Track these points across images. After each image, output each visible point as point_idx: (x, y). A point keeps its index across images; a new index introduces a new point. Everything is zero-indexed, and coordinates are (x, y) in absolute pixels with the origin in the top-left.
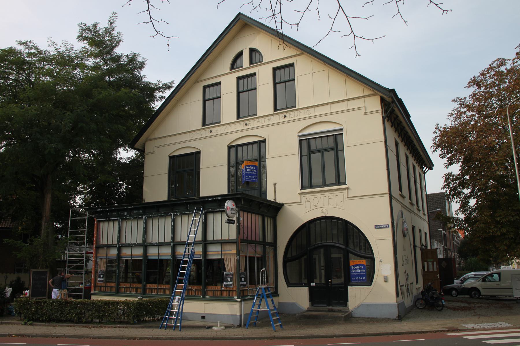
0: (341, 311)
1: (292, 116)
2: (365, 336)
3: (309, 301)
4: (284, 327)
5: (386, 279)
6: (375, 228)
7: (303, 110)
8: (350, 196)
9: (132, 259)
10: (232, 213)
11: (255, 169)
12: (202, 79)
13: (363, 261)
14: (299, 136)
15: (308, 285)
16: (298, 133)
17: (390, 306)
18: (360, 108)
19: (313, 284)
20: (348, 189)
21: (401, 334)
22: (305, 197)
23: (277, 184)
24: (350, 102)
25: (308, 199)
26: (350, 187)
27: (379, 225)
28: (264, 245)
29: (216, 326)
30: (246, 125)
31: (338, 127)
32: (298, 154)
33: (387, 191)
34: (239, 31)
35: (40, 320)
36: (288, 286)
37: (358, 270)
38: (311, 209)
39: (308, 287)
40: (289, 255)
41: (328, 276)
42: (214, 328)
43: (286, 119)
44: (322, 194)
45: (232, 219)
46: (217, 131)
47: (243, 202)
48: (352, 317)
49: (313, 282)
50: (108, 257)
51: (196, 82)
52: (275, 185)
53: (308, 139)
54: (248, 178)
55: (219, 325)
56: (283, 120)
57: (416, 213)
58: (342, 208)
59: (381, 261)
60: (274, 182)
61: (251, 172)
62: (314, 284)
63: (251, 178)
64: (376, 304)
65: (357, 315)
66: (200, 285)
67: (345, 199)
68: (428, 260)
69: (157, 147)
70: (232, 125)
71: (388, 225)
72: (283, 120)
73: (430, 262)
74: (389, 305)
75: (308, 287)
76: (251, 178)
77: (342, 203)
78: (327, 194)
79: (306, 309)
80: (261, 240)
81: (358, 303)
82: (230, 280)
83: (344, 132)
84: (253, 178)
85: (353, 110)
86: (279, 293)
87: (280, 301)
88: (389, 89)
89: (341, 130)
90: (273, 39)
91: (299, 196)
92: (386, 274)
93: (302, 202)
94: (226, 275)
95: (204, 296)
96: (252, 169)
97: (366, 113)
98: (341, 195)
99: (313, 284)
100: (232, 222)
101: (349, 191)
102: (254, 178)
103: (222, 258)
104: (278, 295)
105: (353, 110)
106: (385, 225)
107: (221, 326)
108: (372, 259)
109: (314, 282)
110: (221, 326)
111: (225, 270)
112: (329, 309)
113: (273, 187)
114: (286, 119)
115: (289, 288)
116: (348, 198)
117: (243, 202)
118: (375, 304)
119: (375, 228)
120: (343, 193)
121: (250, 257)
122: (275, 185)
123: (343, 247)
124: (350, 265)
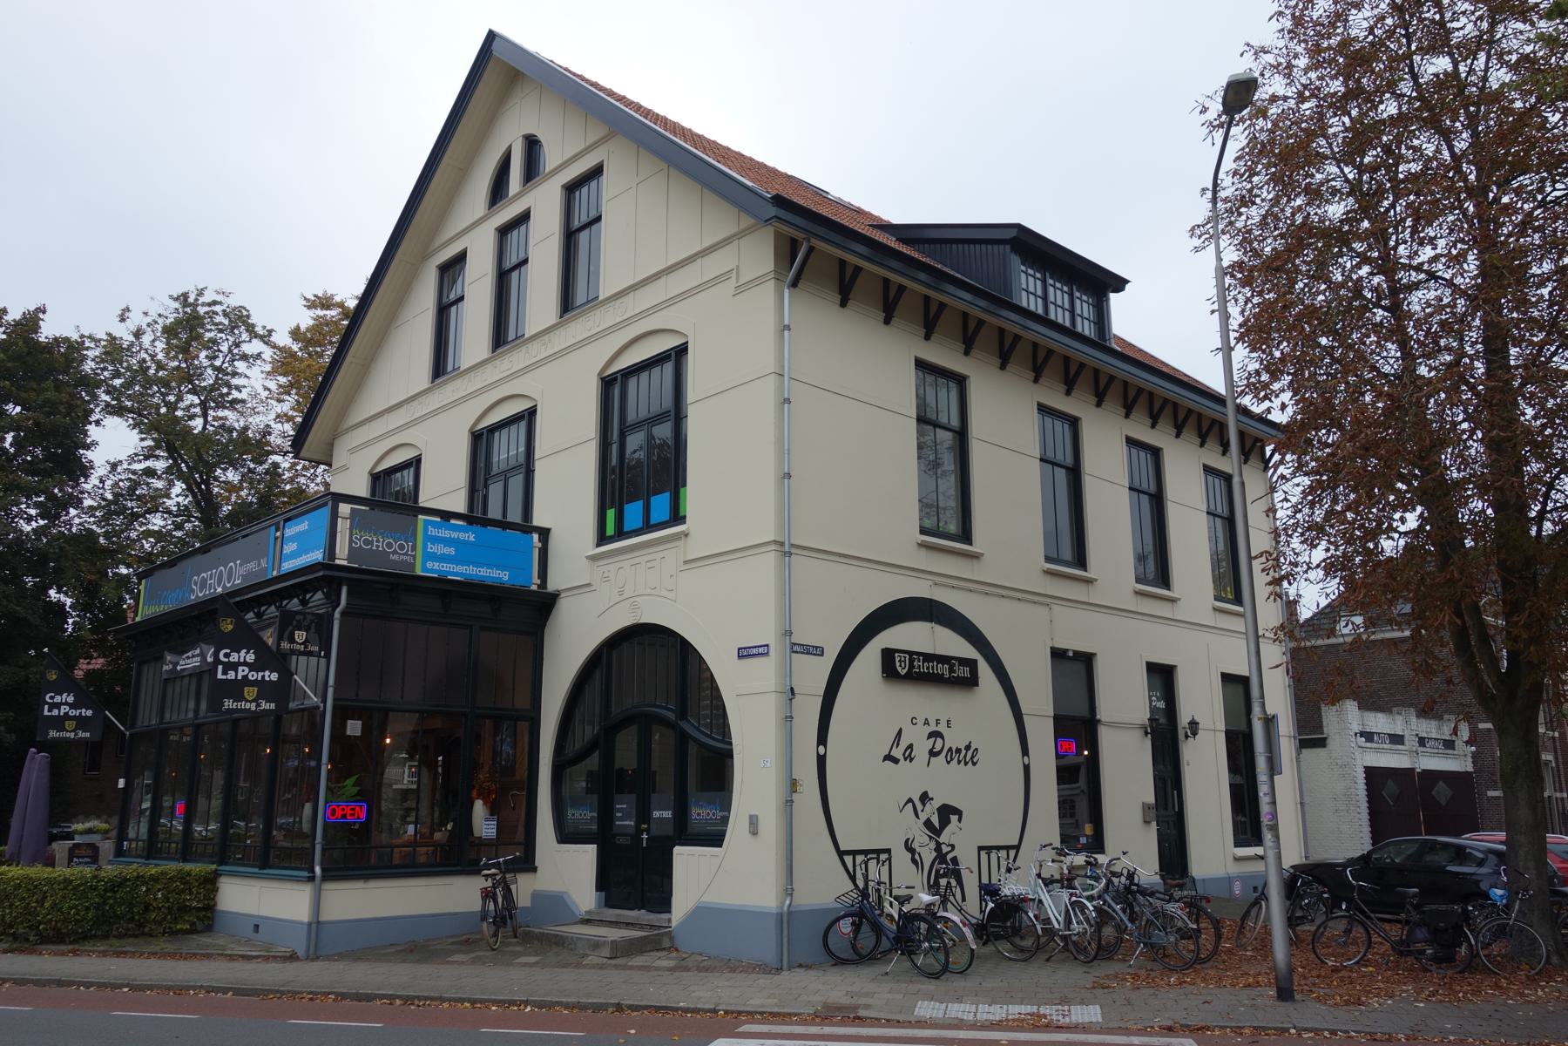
25: (606, 575)
51: (426, 256)
58: (671, 595)
78: (642, 557)
97: (740, 290)
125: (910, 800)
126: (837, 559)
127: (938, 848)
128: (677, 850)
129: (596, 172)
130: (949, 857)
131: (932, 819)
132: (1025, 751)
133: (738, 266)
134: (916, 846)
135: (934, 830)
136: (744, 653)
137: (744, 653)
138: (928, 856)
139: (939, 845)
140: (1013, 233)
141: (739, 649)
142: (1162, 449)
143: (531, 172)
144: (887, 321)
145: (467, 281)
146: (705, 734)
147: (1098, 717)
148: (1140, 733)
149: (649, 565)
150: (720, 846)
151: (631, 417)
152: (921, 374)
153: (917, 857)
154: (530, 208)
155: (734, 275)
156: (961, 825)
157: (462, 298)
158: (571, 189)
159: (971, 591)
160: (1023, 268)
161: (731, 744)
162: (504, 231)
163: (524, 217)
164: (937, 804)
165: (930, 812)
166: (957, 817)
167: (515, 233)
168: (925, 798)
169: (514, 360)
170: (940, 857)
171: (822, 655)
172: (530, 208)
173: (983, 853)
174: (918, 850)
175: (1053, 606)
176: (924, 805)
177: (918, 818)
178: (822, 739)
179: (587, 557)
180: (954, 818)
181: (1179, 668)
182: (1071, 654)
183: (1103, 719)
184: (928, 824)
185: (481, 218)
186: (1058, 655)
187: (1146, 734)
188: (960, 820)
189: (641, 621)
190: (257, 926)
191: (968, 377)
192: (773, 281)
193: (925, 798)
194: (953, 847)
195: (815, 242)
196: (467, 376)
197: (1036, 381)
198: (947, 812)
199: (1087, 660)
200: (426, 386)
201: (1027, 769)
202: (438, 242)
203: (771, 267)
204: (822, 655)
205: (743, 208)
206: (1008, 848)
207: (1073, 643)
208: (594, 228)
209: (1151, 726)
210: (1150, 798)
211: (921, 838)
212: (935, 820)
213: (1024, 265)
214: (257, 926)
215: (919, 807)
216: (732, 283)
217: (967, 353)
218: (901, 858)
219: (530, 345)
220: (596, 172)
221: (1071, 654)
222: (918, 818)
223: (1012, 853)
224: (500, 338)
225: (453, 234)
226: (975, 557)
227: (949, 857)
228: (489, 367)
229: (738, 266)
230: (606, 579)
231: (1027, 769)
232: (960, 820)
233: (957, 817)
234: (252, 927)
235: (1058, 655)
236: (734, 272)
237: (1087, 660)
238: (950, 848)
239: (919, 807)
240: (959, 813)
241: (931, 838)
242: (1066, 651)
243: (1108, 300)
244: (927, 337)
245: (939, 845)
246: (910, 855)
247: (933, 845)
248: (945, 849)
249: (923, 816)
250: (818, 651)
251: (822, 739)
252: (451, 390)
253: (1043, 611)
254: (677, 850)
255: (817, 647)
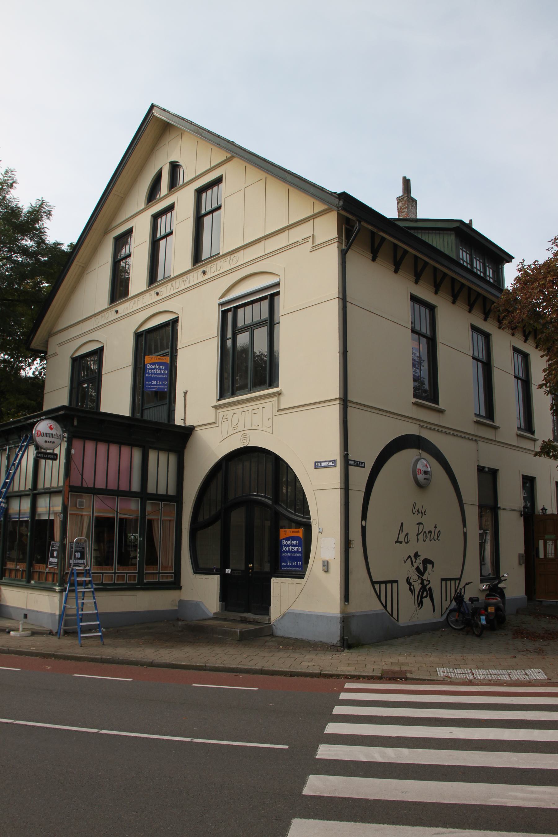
0: (257, 622)
1: (213, 270)
2: (205, 670)
3: (220, 601)
4: (106, 641)
5: (326, 567)
6: (316, 468)
7: (228, 257)
8: (281, 407)
9: (21, 519)
10: (46, 442)
11: (164, 370)
12: (113, 226)
13: (299, 532)
14: (221, 305)
15: (220, 572)
16: (220, 299)
17: (327, 618)
18: (305, 240)
19: (228, 571)
20: (279, 394)
21: (276, 675)
22: (222, 412)
23: (188, 393)
24: (293, 231)
25: (225, 417)
26: (283, 391)
27: (320, 462)
28: (141, 498)
29: (17, 630)
30: (157, 294)
31: (271, 280)
32: (218, 336)
33: (335, 392)
34: (160, 138)
35: (483, 627)
36: (303, 578)
37: (292, 548)
38: (229, 435)
39: (219, 576)
40: (200, 519)
41: (249, 559)
42: (12, 633)
43: (207, 277)
44: (245, 405)
45: (51, 451)
46: (124, 309)
47: (76, 423)
48: (272, 635)
49: (228, 568)
50: (21, 516)
51: (106, 232)
52: (185, 393)
53: (234, 307)
54: (151, 385)
55: (21, 629)
56: (201, 278)
57: (516, 444)
58: (270, 430)
59: (321, 531)
60: (185, 390)
61: (156, 374)
62: (230, 570)
63: (157, 385)
64: (309, 613)
65: (279, 632)
66: (43, 564)
67: (274, 415)
68: (547, 537)
69: (60, 345)
70: (141, 297)
71: (335, 461)
72: (201, 278)
73: (550, 540)
74: (327, 617)
75: (219, 576)
76: (157, 385)
77: (271, 420)
78: (249, 406)
79: (211, 615)
80: (136, 487)
81: (284, 610)
82: (79, 557)
83: (281, 289)
84: (160, 385)
85: (296, 244)
86: (183, 583)
87: (182, 598)
88: (338, 193)
89: (277, 285)
90: (199, 140)
91: (213, 410)
92: (327, 558)
93: (218, 423)
94: (53, 547)
95: (29, 582)
96: (159, 369)
97: (315, 248)
98: (269, 405)
99: (228, 571)
100: (52, 457)
101: (282, 398)
102: (162, 385)
103: (50, 518)
104: (180, 588)
105: (296, 244)
106: (330, 461)
107: (24, 630)
108: (308, 527)
109: (231, 566)
110: (24, 630)
111: (53, 539)
112: (241, 617)
113: (183, 398)
114: (207, 277)
115: (198, 576)
116: (279, 410)
117: (76, 423)
118: (307, 614)
119: (316, 468)
120: (272, 402)
121: (121, 520)
122: (185, 393)
123: (270, 502)
124: (281, 538)
125: (410, 557)
126: (379, 412)
127: (422, 583)
128: (273, 580)
129: (218, 181)
130: (428, 587)
131: (420, 566)
132: (464, 525)
133: (313, 235)
134: (412, 581)
135: (421, 572)
136: (318, 465)
137: (318, 465)
138: (417, 587)
139: (423, 581)
140: (457, 225)
141: (315, 463)
142: (529, 354)
143: (173, 184)
144: (396, 271)
145: (133, 245)
146: (291, 513)
147: (499, 506)
148: (517, 514)
149: (254, 412)
150: (303, 578)
151: (240, 324)
152: (412, 303)
153: (412, 587)
154: (174, 203)
155: (311, 239)
156: (433, 570)
157: (129, 256)
158: (200, 192)
159: (455, 435)
160: (461, 247)
161: (310, 519)
162: (156, 217)
163: (171, 208)
164: (422, 558)
165: (418, 563)
166: (431, 565)
167: (164, 218)
168: (416, 555)
169: (165, 290)
170: (423, 588)
171: (364, 467)
172: (174, 203)
173: (444, 583)
174: (413, 583)
175: (479, 442)
176: (416, 559)
177: (413, 566)
178: (364, 517)
179: (213, 407)
180: (429, 566)
181: (500, 471)
182: (486, 469)
183: (502, 507)
184: (418, 569)
185: (143, 209)
186: (481, 469)
187: (521, 515)
188: (433, 567)
189: (249, 445)
190: (26, 616)
191: (437, 306)
192: (337, 243)
193: (416, 555)
194: (429, 581)
195: (363, 223)
196: (133, 301)
197: (470, 311)
198: (426, 562)
199: (494, 473)
200: (106, 307)
201: (465, 534)
202: (114, 224)
203: (335, 234)
204: (364, 467)
205: (322, 200)
206: (455, 579)
207: (488, 464)
208: (215, 214)
209: (524, 511)
210: (522, 551)
211: (414, 577)
212: (421, 567)
213: (461, 246)
214: (26, 616)
215: (414, 560)
216: (310, 244)
217: (436, 293)
218: (404, 586)
219: (174, 282)
220: (218, 181)
221: (486, 469)
222: (413, 566)
223: (457, 582)
224: (153, 278)
225: (124, 219)
226: (441, 411)
227: (428, 587)
228: (147, 295)
229: (313, 235)
230: (225, 419)
231: (465, 534)
232: (433, 567)
233: (431, 565)
234: (23, 616)
235: (481, 469)
236: (311, 238)
237: (494, 473)
238: (428, 582)
239: (414, 560)
240: (432, 563)
241: (419, 577)
242: (484, 468)
243: (502, 268)
244: (416, 282)
245: (423, 581)
246: (408, 586)
247: (420, 581)
248: (426, 583)
249: (415, 565)
250: (362, 465)
251: (364, 517)
252: (124, 307)
253: (472, 445)
254: (273, 580)
255: (361, 462)
